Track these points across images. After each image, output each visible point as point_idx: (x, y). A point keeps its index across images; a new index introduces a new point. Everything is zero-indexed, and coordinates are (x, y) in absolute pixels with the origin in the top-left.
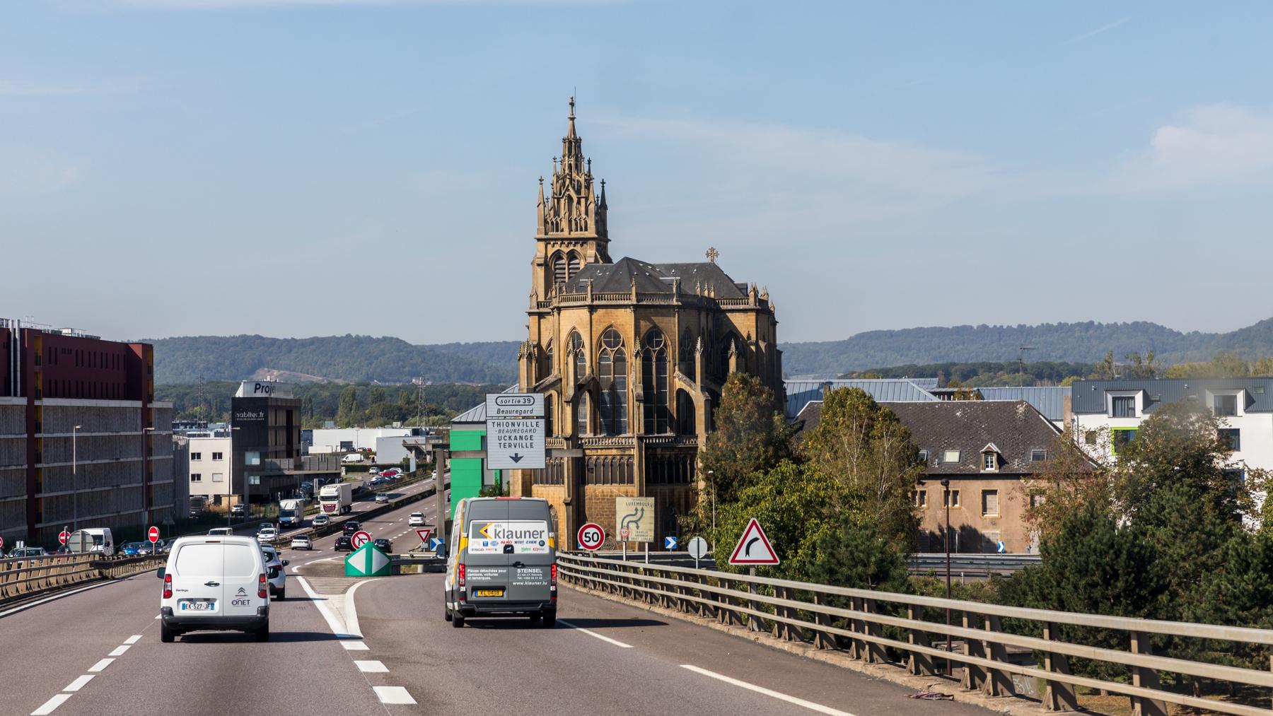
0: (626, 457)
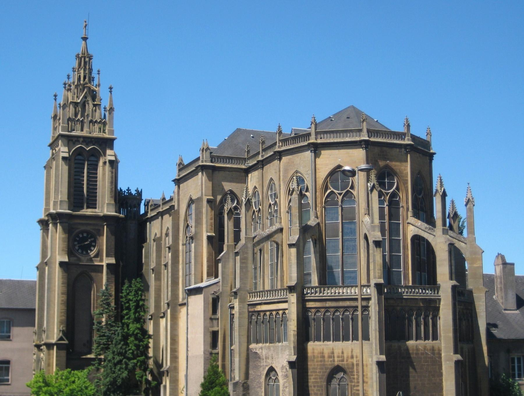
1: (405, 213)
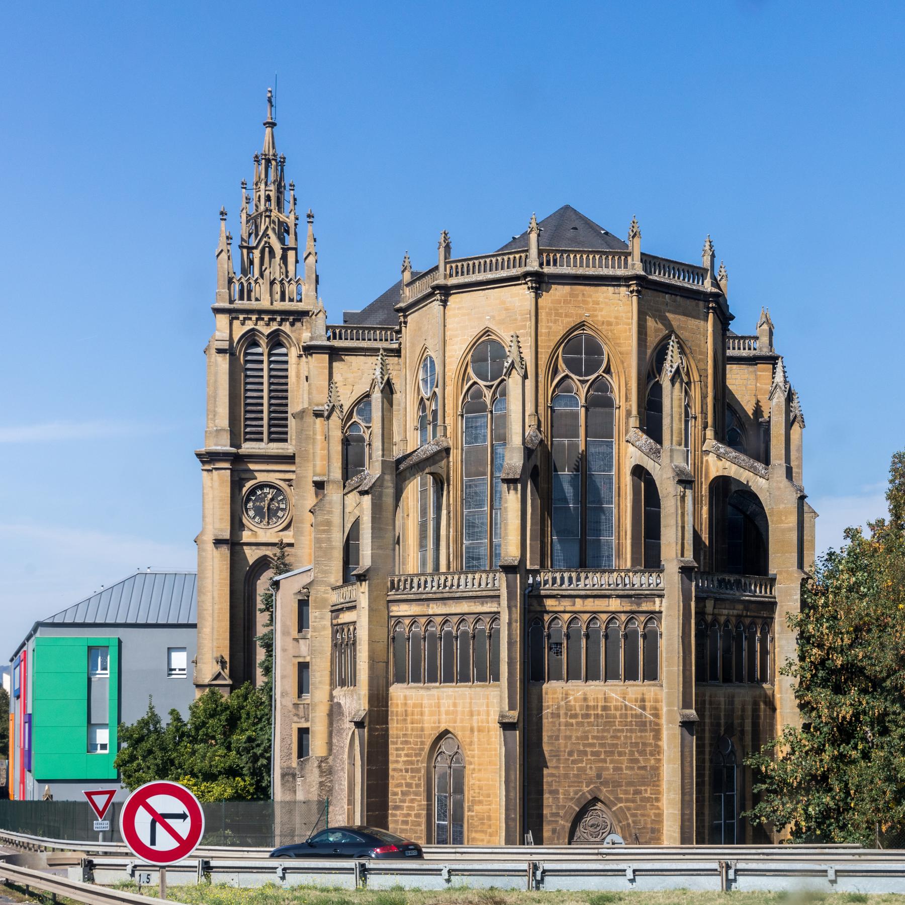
0: (642, 618)
1: (623, 421)
